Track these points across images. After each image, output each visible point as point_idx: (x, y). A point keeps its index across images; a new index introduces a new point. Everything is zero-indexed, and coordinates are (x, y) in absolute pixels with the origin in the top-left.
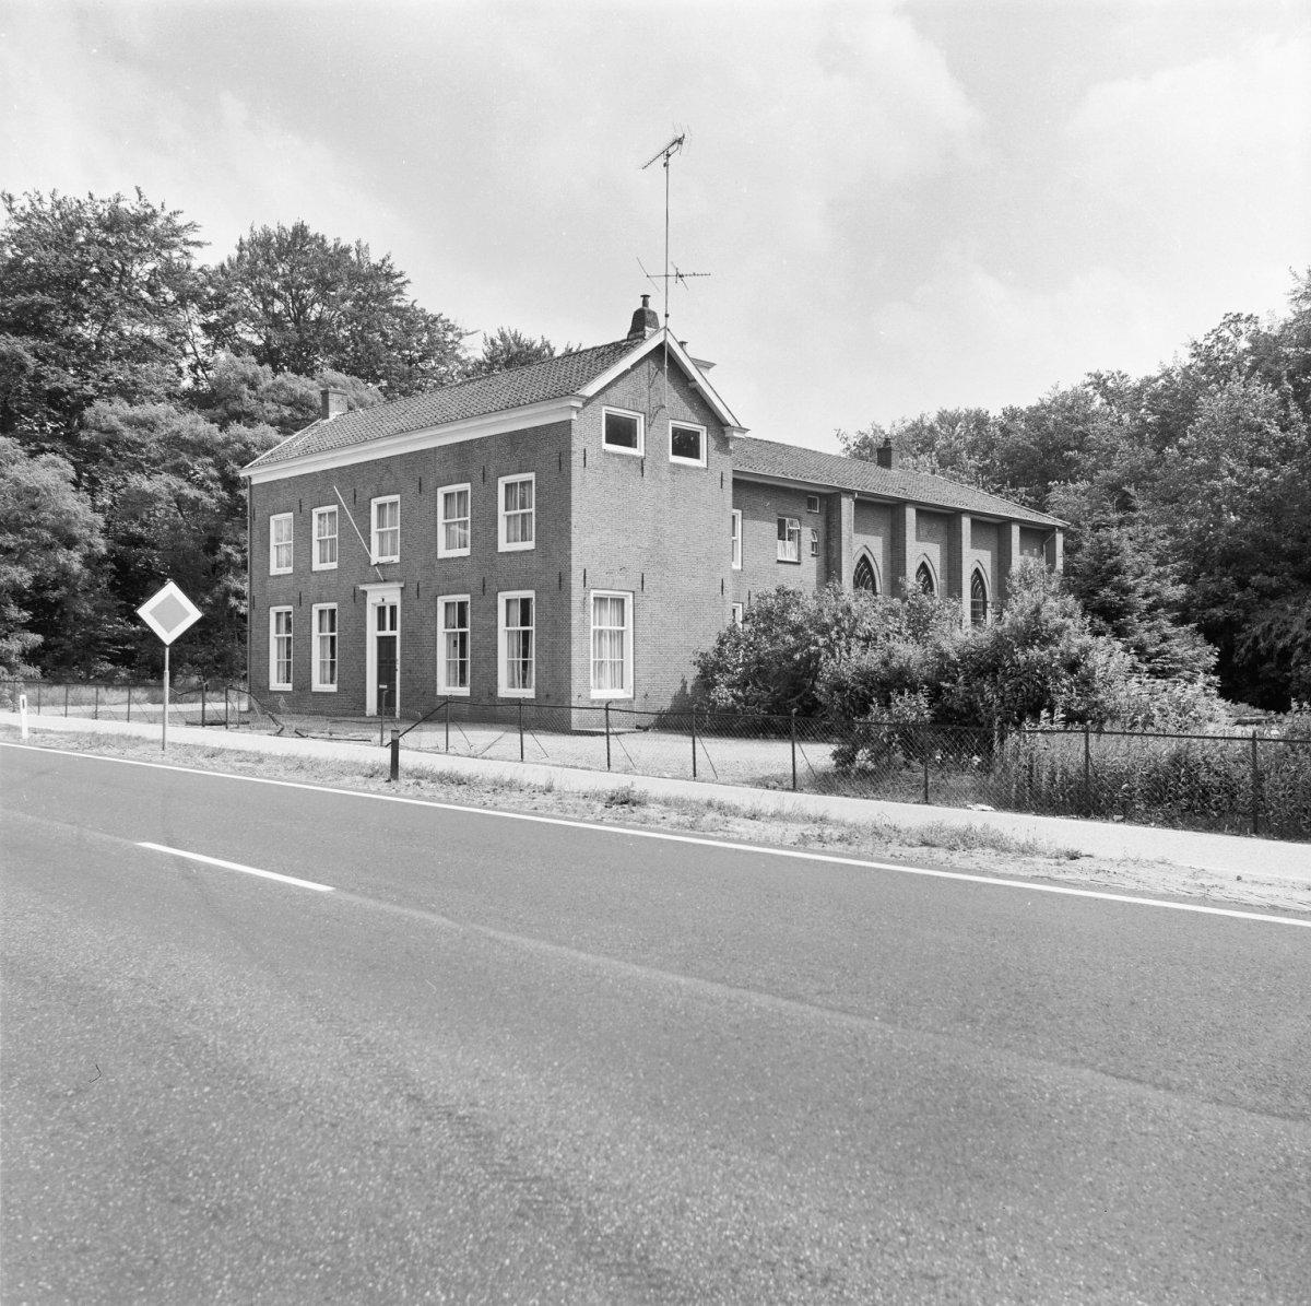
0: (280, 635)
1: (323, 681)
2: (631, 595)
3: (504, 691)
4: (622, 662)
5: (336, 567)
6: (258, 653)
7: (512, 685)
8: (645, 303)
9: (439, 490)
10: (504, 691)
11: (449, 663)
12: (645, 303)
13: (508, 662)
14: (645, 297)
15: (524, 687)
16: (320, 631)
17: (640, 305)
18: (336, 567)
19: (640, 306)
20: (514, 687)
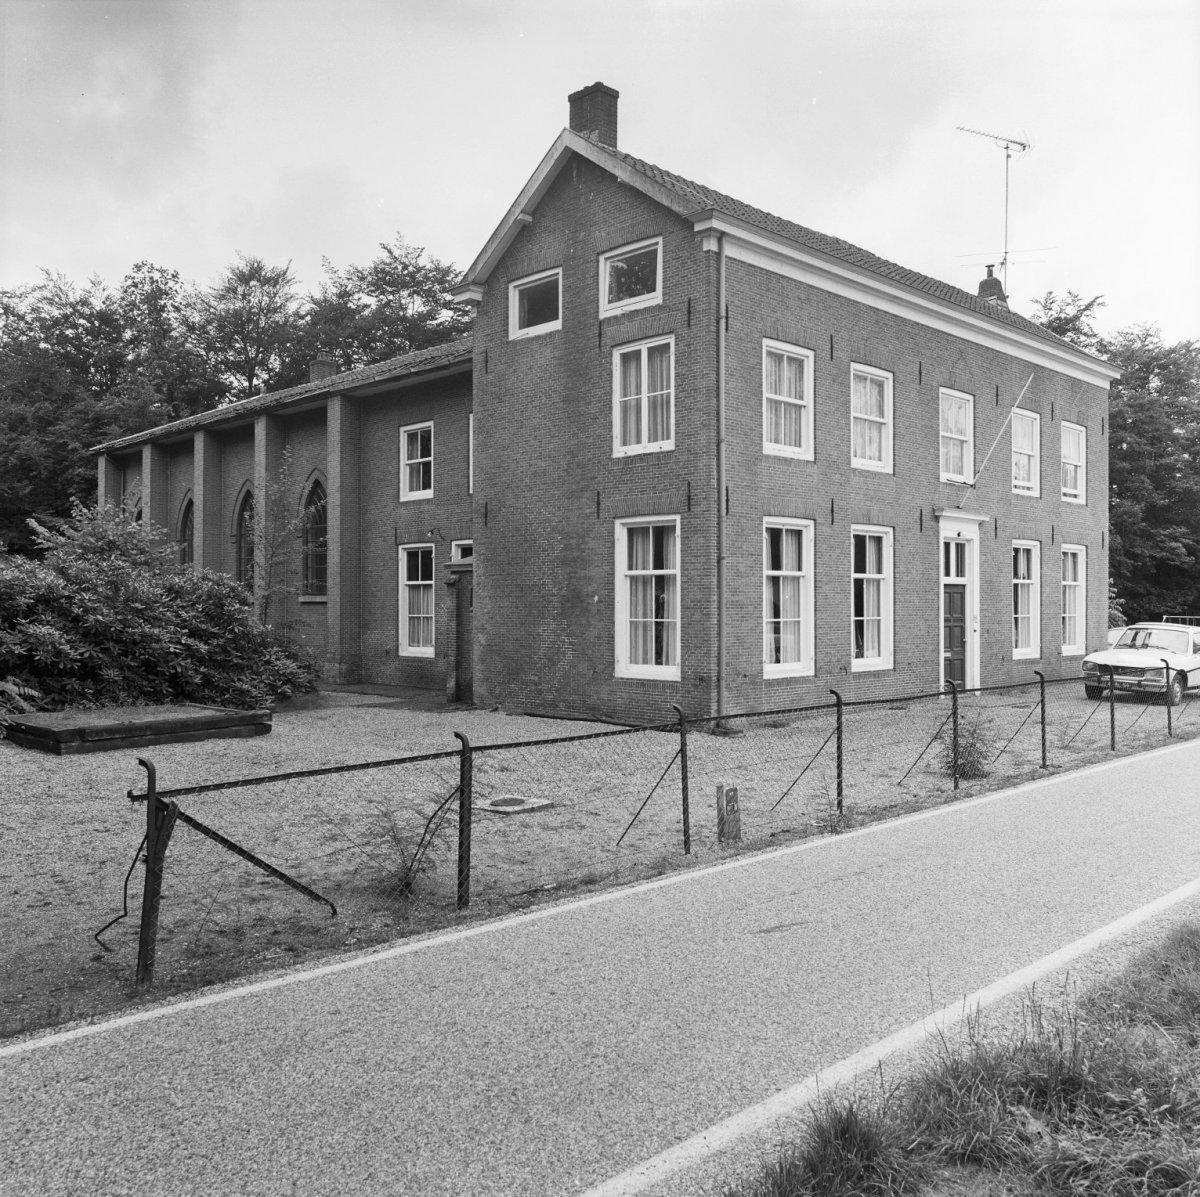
0: (634, 573)
1: (634, 660)
2: (891, 530)
3: (626, 668)
4: (879, 621)
5: (431, 496)
6: (739, 605)
7: (634, 660)
8: (990, 273)
9: (402, 429)
10: (626, 668)
11: (634, 625)
12: (990, 273)
13: (631, 622)
14: (990, 267)
15: (659, 662)
16: (630, 568)
17: (984, 276)
18: (431, 496)
19: (985, 277)
20: (661, 663)
